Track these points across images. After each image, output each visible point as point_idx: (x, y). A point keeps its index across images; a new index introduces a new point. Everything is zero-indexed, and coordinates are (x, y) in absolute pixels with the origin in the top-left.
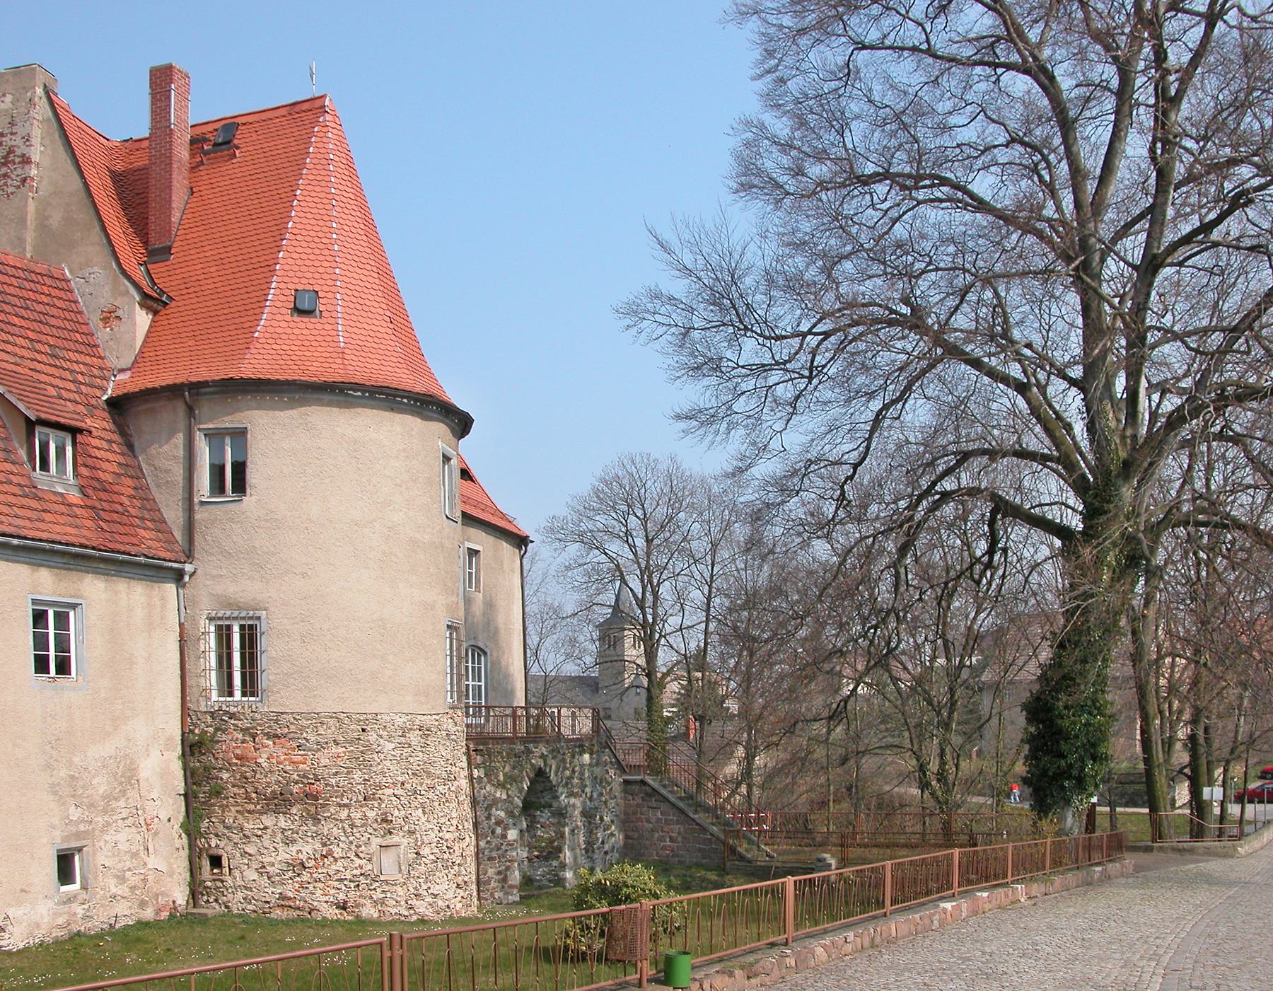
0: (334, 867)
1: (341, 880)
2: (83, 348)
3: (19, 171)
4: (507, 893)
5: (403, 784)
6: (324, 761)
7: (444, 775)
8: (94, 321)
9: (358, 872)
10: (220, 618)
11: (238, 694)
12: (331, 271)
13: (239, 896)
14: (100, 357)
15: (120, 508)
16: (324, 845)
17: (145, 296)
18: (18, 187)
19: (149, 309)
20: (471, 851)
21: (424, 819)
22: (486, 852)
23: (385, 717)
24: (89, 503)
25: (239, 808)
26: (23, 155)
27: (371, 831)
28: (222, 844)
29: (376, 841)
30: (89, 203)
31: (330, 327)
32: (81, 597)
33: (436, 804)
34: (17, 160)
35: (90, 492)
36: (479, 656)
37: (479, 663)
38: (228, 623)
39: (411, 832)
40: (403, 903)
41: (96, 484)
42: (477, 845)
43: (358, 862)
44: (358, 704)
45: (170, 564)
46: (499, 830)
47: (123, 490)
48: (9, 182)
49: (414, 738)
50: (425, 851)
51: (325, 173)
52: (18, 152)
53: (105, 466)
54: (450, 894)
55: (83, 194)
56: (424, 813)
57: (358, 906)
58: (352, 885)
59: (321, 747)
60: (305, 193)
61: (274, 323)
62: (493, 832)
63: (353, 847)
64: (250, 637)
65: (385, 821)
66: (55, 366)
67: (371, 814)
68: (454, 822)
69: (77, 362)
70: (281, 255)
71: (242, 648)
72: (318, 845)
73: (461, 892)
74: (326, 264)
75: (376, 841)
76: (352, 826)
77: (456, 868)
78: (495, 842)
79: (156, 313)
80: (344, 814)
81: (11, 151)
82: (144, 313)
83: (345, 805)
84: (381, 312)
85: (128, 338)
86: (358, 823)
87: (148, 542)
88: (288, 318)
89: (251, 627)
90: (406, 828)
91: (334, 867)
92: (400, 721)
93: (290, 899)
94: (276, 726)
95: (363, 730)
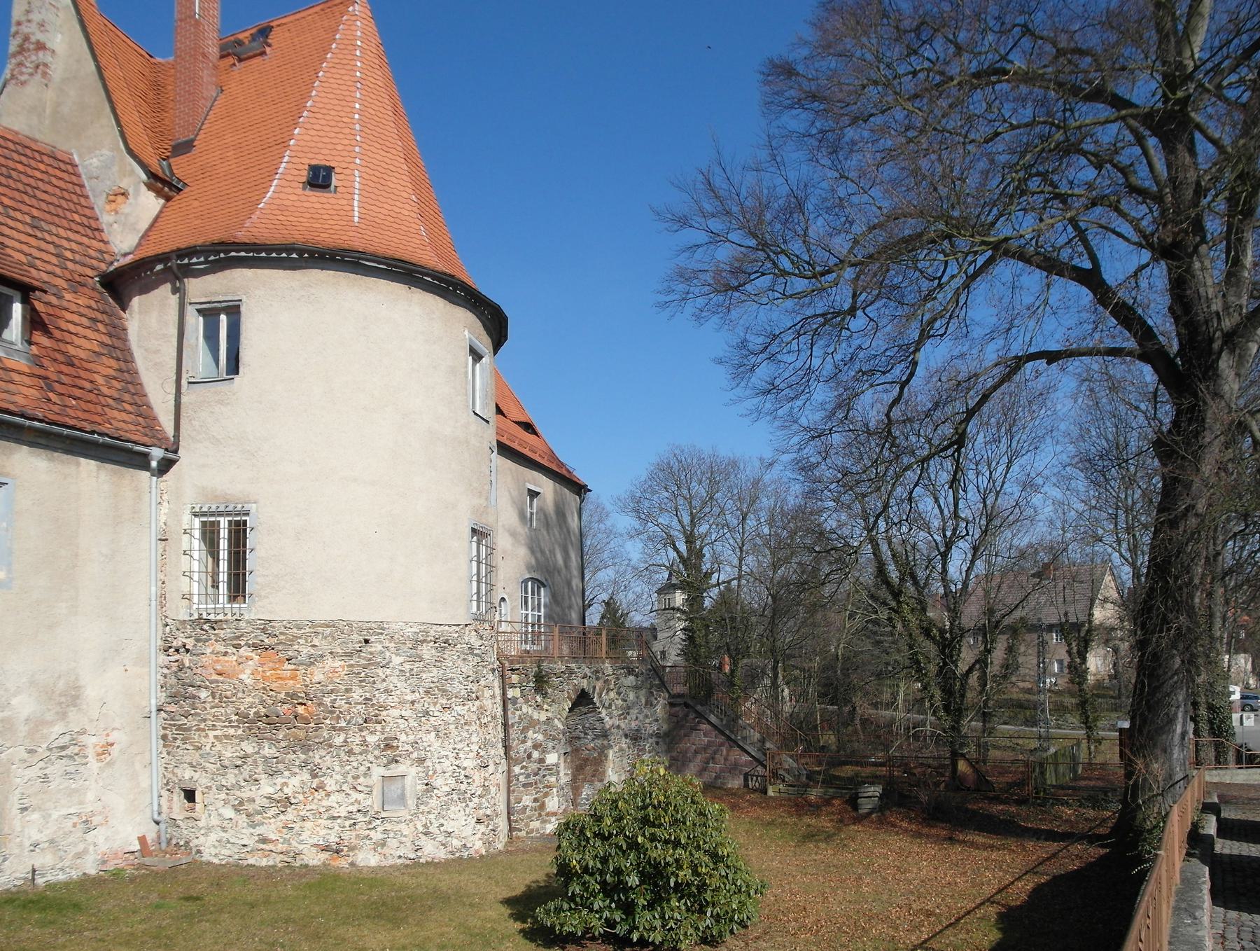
0: (325, 803)
1: (334, 818)
2: (80, 229)
3: (34, 58)
4: (544, 822)
5: (413, 703)
6: (318, 677)
7: (464, 692)
8: (99, 203)
9: (354, 808)
10: (204, 515)
11: (223, 598)
12: (351, 148)
13: (213, 837)
14: (102, 241)
15: (88, 385)
16: (314, 776)
17: (152, 176)
18: (31, 75)
19: (159, 193)
20: (500, 778)
21: (437, 744)
22: (522, 778)
23: (393, 626)
24: (41, 372)
25: (218, 733)
26: (38, 42)
27: (372, 759)
28: (196, 776)
29: (378, 771)
30: (100, 85)
31: (345, 202)
32: (7, 475)
33: (452, 727)
34: (32, 47)
35: (46, 363)
36: (539, 588)
37: (539, 594)
38: (212, 519)
39: (421, 761)
40: (408, 844)
41: (60, 357)
42: (509, 771)
43: (355, 795)
44: (360, 611)
45: (129, 445)
46: (536, 755)
47: (100, 368)
48: (24, 70)
49: (427, 651)
50: (438, 782)
51: (350, 57)
52: (33, 39)
53: (77, 341)
54: (468, 831)
55: (96, 77)
56: (438, 736)
57: (352, 849)
58: (348, 823)
59: (313, 661)
60: (328, 75)
61: (281, 195)
62: (529, 756)
63: (349, 778)
64: (239, 532)
65: (388, 747)
66: (35, 237)
67: (372, 739)
68: (475, 747)
69: (67, 239)
70: (296, 131)
71: (230, 543)
72: (306, 776)
73: (482, 828)
74: (346, 142)
75: (378, 771)
76: (350, 752)
77: (476, 800)
78: (534, 766)
79: (168, 199)
80: (338, 740)
81: (26, 39)
82: (152, 195)
83: (341, 729)
84: (405, 195)
85: (132, 220)
86: (357, 749)
87: (119, 422)
88: (300, 191)
89: (238, 523)
90: (415, 755)
91: (325, 803)
92: (409, 631)
93: (271, 841)
94: (264, 637)
95: (367, 641)
